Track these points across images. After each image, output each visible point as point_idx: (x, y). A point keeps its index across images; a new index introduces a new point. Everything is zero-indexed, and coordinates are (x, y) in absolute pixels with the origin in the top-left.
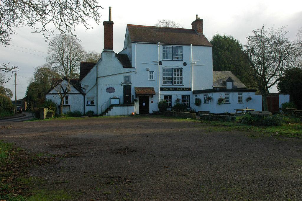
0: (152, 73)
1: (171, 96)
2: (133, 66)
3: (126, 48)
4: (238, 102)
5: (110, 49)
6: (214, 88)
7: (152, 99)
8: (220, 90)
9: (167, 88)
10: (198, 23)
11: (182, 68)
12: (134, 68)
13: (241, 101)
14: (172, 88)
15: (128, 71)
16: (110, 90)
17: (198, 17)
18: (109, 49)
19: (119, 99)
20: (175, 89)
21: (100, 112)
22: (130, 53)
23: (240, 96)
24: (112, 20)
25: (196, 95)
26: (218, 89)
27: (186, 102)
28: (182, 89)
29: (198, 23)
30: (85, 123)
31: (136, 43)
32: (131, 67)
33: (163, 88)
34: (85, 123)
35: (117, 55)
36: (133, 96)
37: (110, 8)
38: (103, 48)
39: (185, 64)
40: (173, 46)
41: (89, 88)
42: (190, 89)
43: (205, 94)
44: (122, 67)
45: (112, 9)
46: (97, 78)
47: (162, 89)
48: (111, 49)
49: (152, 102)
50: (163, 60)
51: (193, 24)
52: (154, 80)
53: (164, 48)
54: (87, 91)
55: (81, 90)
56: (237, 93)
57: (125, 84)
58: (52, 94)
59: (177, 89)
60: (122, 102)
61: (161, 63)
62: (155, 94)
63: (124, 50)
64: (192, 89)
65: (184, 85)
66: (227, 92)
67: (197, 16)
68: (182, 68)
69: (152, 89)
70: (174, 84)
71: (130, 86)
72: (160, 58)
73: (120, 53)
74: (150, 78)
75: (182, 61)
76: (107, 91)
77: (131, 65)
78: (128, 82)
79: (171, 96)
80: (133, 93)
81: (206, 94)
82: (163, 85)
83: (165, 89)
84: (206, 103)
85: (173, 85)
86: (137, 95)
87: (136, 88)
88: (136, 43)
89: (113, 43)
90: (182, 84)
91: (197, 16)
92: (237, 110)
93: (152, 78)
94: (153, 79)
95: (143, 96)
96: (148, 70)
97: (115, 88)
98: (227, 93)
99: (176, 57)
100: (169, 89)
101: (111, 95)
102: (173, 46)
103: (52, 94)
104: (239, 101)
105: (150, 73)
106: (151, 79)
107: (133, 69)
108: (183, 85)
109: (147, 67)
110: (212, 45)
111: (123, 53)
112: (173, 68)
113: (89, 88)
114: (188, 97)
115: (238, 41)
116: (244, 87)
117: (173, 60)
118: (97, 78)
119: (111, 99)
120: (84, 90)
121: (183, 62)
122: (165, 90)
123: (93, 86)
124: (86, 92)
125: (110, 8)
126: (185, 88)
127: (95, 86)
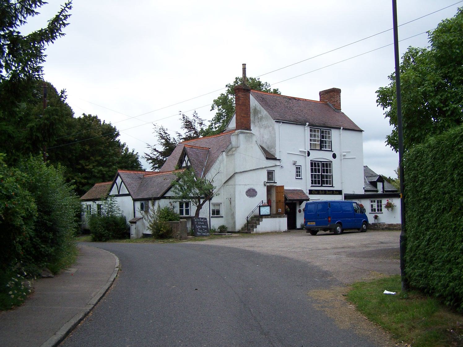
5: (248, 130)
10: (42, 29)
11: (331, 162)
12: (280, 160)
16: (251, 193)
21: (239, 227)
29: (42, 29)
31: (281, 122)
37: (244, 65)
39: (334, 156)
40: (320, 129)
42: (339, 192)
51: (323, 94)
57: (268, 184)
58: (170, 198)
59: (327, 192)
64: (343, 193)
66: (380, 198)
68: (331, 162)
69: (301, 191)
70: (323, 185)
72: (308, 148)
75: (331, 151)
76: (246, 194)
82: (312, 186)
85: (322, 186)
90: (331, 185)
95: (291, 202)
97: (257, 190)
99: (323, 145)
103: (170, 198)
107: (277, 161)
108: (332, 186)
112: (321, 162)
116: (123, 184)
117: (321, 150)
119: (260, 207)
121: (332, 153)
125: (244, 65)
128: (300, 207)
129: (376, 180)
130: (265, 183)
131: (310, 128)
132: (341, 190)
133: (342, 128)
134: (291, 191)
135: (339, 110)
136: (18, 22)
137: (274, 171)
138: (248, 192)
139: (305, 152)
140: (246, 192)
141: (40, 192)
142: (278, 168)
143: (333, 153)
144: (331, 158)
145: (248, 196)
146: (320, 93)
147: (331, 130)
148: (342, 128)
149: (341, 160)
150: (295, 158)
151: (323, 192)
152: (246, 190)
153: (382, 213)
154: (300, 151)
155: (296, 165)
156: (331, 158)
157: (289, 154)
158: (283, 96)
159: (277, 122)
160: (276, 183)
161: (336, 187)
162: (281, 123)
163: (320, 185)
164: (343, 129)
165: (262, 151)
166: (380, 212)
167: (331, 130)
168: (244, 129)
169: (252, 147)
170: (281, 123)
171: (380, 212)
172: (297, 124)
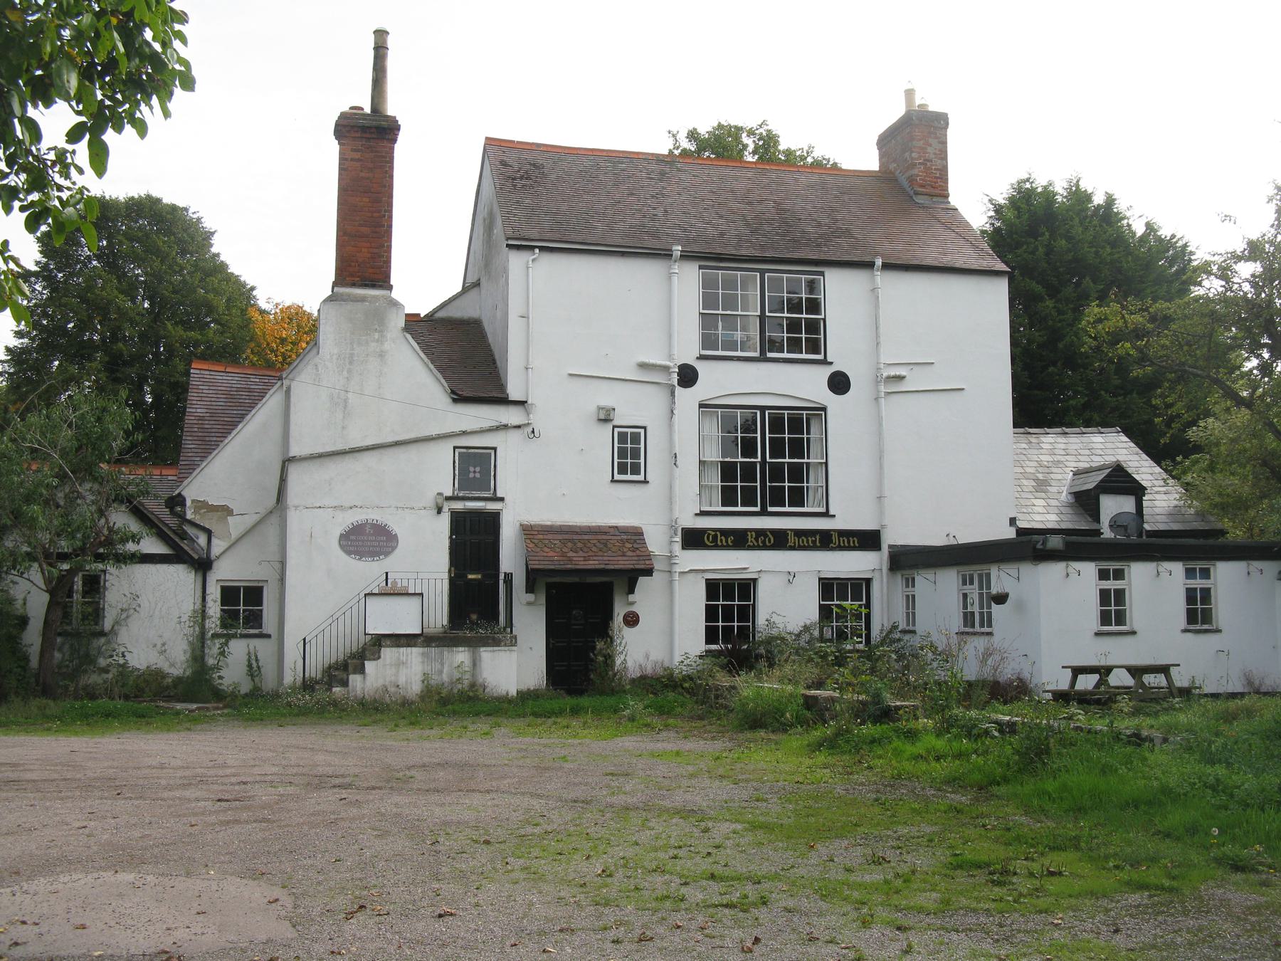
0: (636, 439)
1: (755, 580)
2: (514, 393)
3: (477, 284)
4: (1182, 620)
5: (373, 286)
6: (1021, 532)
7: (631, 598)
8: (1068, 545)
9: (725, 532)
13: (1207, 617)
14: (760, 533)
15: (486, 425)
17: (918, 101)
18: (365, 286)
19: (417, 600)
20: (779, 540)
22: (499, 314)
23: (1198, 583)
24: (391, 109)
25: (907, 572)
26: (1055, 542)
27: (835, 624)
28: (824, 541)
30: (669, 746)
31: (533, 248)
32: (504, 401)
33: (702, 532)
34: (669, 746)
35: (413, 323)
36: (509, 578)
37: (381, 35)
38: (948, 133)
39: (839, 383)
40: (762, 272)
41: (236, 525)
42: (868, 540)
43: (968, 570)
44: (449, 400)
45: (391, 42)
46: (287, 461)
47: (693, 539)
48: (381, 287)
49: (632, 620)
50: (702, 358)
52: (645, 482)
53: (707, 284)
54: (218, 546)
55: (184, 536)
56: (1177, 568)
57: (459, 506)
59: (792, 540)
60: (439, 616)
61: (688, 376)
62: (649, 572)
63: (466, 289)
64: (889, 539)
65: (831, 513)
67: (909, 94)
69: (634, 536)
71: (494, 519)
72: (688, 350)
73: (440, 315)
74: (623, 469)
75: (825, 362)
76: (342, 547)
77: (502, 387)
78: (477, 494)
79: (755, 580)
80: (510, 558)
81: (975, 570)
82: (703, 514)
83: (715, 537)
84: (977, 628)
85: (764, 512)
86: (533, 578)
87: (529, 532)
88: (533, 248)
89: (390, 247)
91: (909, 94)
92: (1077, 671)
93: (636, 470)
94: (638, 473)
96: (606, 420)
97: (395, 528)
98: (1112, 566)
100: (738, 540)
101: (369, 572)
102: (762, 272)
104: (1192, 617)
105: (623, 437)
106: (629, 477)
108: (826, 514)
109: (607, 402)
110: (1001, 266)
111: (455, 312)
113: (236, 525)
114: (859, 587)
115: (1185, 246)
117: (763, 359)
118: (287, 461)
120: (202, 540)
121: (825, 372)
122: (716, 547)
123: (263, 511)
124: (216, 551)
125: (381, 35)
126: (842, 533)
127: (271, 512)
128: (632, 603)
129: (1090, 486)
130: (440, 500)
131: (700, 267)
132: (878, 532)
133: (879, 262)
134: (577, 533)
135: (941, 199)
136: (151, 108)
137: (495, 449)
138: (352, 537)
139: (666, 369)
140: (342, 535)
141: (81, 268)
142: (514, 436)
143: (828, 371)
144: (821, 394)
145: (349, 553)
146: (946, 115)
147: (822, 274)
148: (879, 262)
149: (876, 399)
150: (607, 396)
151: (766, 536)
152: (338, 531)
153: (1134, 633)
154: (643, 366)
155: (616, 422)
156: (821, 394)
157: (576, 379)
158: (604, 154)
159: (518, 247)
160: (502, 499)
161: (846, 518)
162: (537, 251)
163: (757, 509)
164: (887, 266)
165: (428, 366)
166: (1113, 628)
167: (822, 274)
168: (353, 285)
169: (382, 355)
170: (537, 251)
171: (1113, 628)
172: (623, 254)
